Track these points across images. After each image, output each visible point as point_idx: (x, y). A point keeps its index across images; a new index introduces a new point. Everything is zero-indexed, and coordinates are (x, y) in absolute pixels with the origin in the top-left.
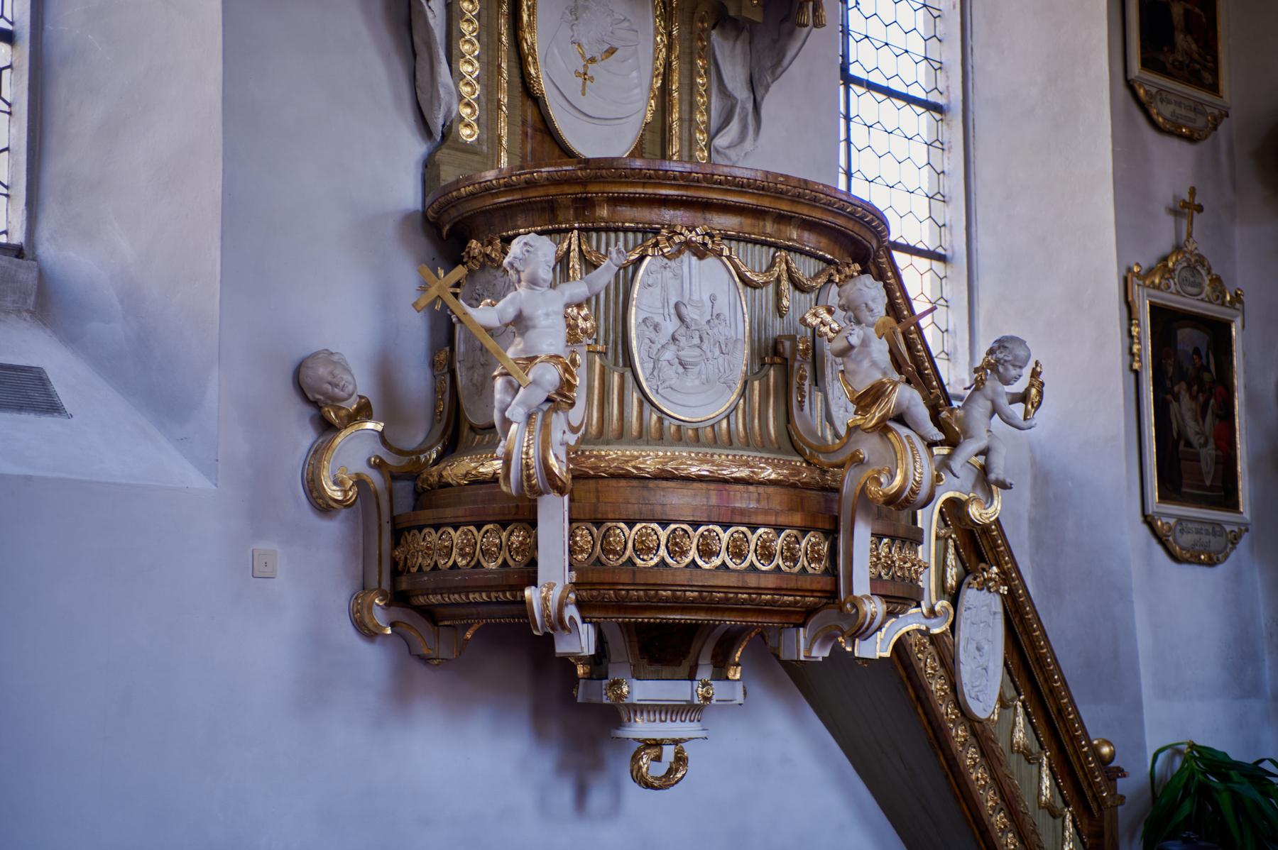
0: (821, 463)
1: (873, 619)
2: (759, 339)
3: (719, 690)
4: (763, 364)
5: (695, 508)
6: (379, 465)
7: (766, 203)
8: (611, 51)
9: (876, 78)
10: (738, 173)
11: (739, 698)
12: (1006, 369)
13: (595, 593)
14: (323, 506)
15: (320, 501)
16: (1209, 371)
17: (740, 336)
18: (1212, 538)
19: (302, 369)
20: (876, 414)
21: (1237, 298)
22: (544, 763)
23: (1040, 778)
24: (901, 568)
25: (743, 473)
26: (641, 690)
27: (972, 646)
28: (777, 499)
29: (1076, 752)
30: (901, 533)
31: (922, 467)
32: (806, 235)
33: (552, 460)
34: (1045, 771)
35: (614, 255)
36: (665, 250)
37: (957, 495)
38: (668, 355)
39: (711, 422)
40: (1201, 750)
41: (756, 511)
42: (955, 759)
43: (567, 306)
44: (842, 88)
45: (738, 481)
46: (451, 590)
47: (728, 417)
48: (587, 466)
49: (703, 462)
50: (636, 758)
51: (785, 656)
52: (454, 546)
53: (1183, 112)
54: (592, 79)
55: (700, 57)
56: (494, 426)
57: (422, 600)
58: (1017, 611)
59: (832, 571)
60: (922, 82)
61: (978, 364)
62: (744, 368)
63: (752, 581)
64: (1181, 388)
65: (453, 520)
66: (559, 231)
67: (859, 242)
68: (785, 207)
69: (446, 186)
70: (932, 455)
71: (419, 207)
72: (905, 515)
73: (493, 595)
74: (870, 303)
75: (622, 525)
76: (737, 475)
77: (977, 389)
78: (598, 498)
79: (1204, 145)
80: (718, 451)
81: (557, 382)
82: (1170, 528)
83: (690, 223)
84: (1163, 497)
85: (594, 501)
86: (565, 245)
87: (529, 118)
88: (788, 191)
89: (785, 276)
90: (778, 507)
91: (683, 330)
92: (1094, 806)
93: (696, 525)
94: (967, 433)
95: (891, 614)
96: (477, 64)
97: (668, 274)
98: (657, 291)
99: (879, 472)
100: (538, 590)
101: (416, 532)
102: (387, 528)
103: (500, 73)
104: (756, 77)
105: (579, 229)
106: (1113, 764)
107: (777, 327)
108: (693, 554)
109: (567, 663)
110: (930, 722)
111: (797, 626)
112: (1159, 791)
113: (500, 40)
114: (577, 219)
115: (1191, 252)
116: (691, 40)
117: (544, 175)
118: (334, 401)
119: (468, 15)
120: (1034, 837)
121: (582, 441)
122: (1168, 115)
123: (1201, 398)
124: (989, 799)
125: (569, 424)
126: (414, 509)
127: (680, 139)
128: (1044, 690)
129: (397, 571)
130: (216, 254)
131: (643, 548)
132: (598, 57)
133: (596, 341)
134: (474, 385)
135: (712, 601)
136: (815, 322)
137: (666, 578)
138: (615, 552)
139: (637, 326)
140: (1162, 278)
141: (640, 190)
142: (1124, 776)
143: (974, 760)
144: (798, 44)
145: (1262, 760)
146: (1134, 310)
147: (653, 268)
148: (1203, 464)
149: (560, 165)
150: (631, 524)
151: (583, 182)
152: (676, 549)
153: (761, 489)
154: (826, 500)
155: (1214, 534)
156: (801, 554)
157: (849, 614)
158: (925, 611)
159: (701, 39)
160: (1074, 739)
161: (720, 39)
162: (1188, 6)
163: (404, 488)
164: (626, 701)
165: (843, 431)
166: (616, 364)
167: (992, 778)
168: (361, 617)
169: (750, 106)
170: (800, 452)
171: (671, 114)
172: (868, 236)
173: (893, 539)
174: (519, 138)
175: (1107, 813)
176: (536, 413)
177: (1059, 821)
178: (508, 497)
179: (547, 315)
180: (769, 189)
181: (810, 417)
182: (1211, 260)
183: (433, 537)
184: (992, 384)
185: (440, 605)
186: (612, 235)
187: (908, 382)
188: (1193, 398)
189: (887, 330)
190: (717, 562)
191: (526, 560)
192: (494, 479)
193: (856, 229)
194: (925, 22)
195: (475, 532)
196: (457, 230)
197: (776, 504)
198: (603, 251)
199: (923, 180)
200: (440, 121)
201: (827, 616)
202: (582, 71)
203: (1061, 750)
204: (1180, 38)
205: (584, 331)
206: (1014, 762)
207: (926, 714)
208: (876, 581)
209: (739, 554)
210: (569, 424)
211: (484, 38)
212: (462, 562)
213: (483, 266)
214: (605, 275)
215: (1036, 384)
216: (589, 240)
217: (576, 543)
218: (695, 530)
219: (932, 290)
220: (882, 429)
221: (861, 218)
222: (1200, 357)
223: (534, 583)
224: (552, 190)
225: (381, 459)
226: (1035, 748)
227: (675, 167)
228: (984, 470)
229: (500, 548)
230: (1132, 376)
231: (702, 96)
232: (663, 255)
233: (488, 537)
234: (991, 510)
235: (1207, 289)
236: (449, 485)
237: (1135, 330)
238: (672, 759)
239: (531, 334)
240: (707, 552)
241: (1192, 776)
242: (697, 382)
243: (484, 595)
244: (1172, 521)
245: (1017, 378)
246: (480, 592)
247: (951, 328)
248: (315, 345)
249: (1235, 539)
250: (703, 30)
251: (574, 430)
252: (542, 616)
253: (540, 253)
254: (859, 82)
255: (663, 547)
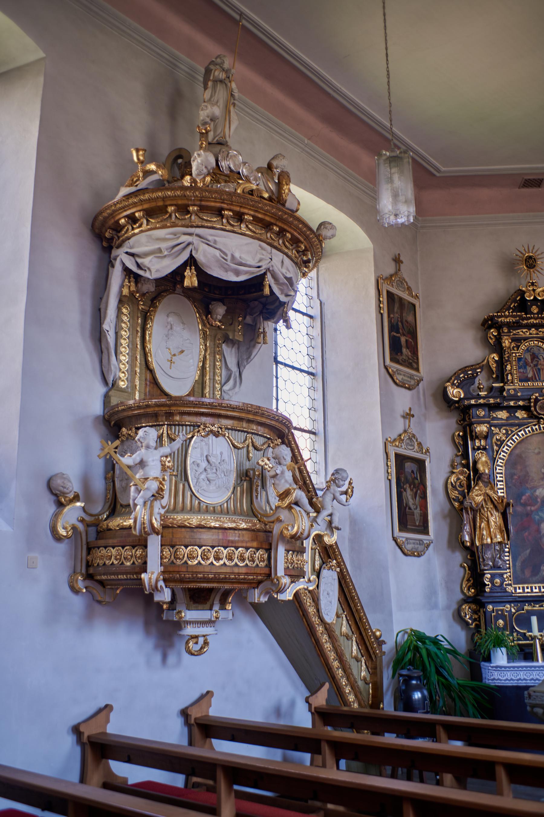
0: (265, 521)
1: (285, 585)
2: (240, 470)
3: (222, 614)
4: (242, 480)
5: (213, 540)
6: (82, 521)
7: (243, 415)
8: (182, 352)
9: (288, 362)
10: (232, 403)
11: (231, 617)
12: (339, 482)
13: (171, 575)
14: (58, 538)
15: (57, 536)
16: (417, 479)
17: (232, 469)
18: (419, 546)
19: (51, 481)
20: (287, 501)
21: (428, 451)
22: (149, 644)
23: (352, 646)
24: (297, 564)
25: (233, 525)
26: (189, 615)
27: (325, 593)
28: (247, 536)
29: (366, 634)
30: (297, 549)
31: (305, 523)
32: (259, 428)
33: (154, 521)
34: (354, 643)
35: (181, 436)
36: (202, 434)
37: (319, 532)
38: (203, 476)
39: (220, 504)
40: (415, 631)
41: (238, 541)
42: (318, 639)
43: (162, 457)
44: (274, 366)
45: (230, 529)
46: (111, 574)
47: (227, 502)
48: (169, 522)
49: (216, 521)
50: (187, 643)
51: (249, 600)
52: (112, 555)
53: (406, 378)
54: (174, 363)
55: (218, 354)
56: (129, 505)
57: (98, 578)
58: (343, 578)
59: (269, 566)
60: (306, 363)
61: (328, 479)
62: (234, 482)
63: (236, 570)
64: (407, 486)
65: (113, 545)
66: (159, 425)
67: (281, 431)
68: (251, 417)
69: (113, 406)
70: (309, 517)
71: (102, 413)
72: (298, 543)
73: (128, 576)
74: (285, 456)
75: (183, 547)
76: (231, 526)
77: (327, 489)
78: (173, 536)
79: (414, 391)
80: (223, 516)
81: (157, 489)
82: (403, 542)
83: (212, 423)
84: (400, 530)
85: (171, 537)
86: (161, 431)
87: (148, 378)
88: (252, 411)
89: (251, 444)
90: (247, 539)
91: (209, 466)
92: (373, 656)
93: (213, 547)
94: (323, 507)
95: (292, 582)
96: (127, 356)
97: (203, 443)
98: (198, 450)
99: (288, 525)
100: (147, 575)
101: (97, 549)
102: (85, 547)
103: (136, 360)
104: (240, 362)
105: (167, 425)
106: (381, 639)
107: (247, 465)
108: (212, 559)
109: (159, 605)
110: (308, 625)
111: (254, 588)
112: (399, 649)
113: (137, 347)
114: (166, 421)
115: (410, 433)
116: (214, 348)
117: (153, 403)
118: (64, 494)
119: (124, 337)
120: (350, 671)
121: (167, 512)
122: (400, 380)
123: (414, 490)
124: (332, 656)
125: (161, 505)
126: (96, 539)
127: (210, 387)
128: (354, 610)
129: (88, 565)
130: (16, 433)
131: (191, 557)
132: (177, 354)
133: (173, 471)
134: (123, 488)
135: (219, 579)
136: (262, 464)
137: (201, 569)
138: (179, 559)
139: (190, 465)
140: (399, 442)
141: (192, 409)
142: (385, 644)
143: (326, 640)
144: (257, 350)
145: (438, 636)
146: (389, 455)
147: (197, 441)
148: (415, 517)
149: (160, 399)
150: (186, 547)
151: (169, 406)
152: (205, 557)
153: (240, 532)
154: (267, 536)
155: (420, 544)
156: (256, 559)
157: (275, 584)
158: (306, 580)
159: (218, 347)
160: (365, 629)
161: (226, 347)
162: (407, 338)
163: (92, 530)
164: (183, 619)
165: (274, 508)
166: (181, 480)
167: (333, 647)
168: (73, 584)
169: (238, 374)
170: (256, 516)
171: (206, 376)
172: (284, 428)
173: (294, 552)
174: (144, 386)
175: (378, 659)
176: (148, 501)
177: (360, 663)
178: (136, 536)
179: (153, 460)
180: (244, 410)
181: (260, 502)
182: (417, 436)
183: (103, 551)
184: (333, 487)
185: (106, 580)
186: (181, 427)
187: (300, 488)
188: (412, 490)
189: (292, 468)
190: (221, 562)
191: (143, 562)
192: (130, 528)
193: (280, 425)
194: (308, 341)
195: (122, 550)
196: (117, 424)
197: (246, 538)
198: (177, 434)
199: (307, 402)
200: (112, 379)
201: (266, 584)
202: (170, 359)
203: (361, 634)
204: (404, 350)
205: (168, 467)
206: (342, 640)
207: (307, 621)
208: (286, 569)
209: (231, 559)
210: (161, 505)
211: (131, 346)
212: (116, 562)
213: (127, 439)
214: (177, 444)
215: (351, 487)
216: (171, 429)
217: (163, 555)
218: (213, 549)
219: (310, 447)
220: (289, 508)
221: (282, 421)
222: (414, 474)
223: (145, 571)
224: (157, 409)
225: (83, 518)
226: (350, 634)
227: (207, 400)
228: (330, 522)
229: (132, 556)
230: (388, 482)
231: (218, 370)
232: (201, 436)
233: (127, 552)
234: (333, 539)
235: (416, 447)
236: (110, 530)
237: (389, 463)
238: (202, 643)
239: (147, 468)
240: (217, 559)
241: (412, 642)
242: (214, 488)
243: (125, 576)
244: (404, 540)
245: (343, 485)
246: (123, 575)
247: (317, 461)
248: (55, 471)
249: (428, 546)
250: (219, 344)
251: (163, 508)
252: (149, 586)
253: (151, 435)
254: (282, 363)
255: (199, 557)
